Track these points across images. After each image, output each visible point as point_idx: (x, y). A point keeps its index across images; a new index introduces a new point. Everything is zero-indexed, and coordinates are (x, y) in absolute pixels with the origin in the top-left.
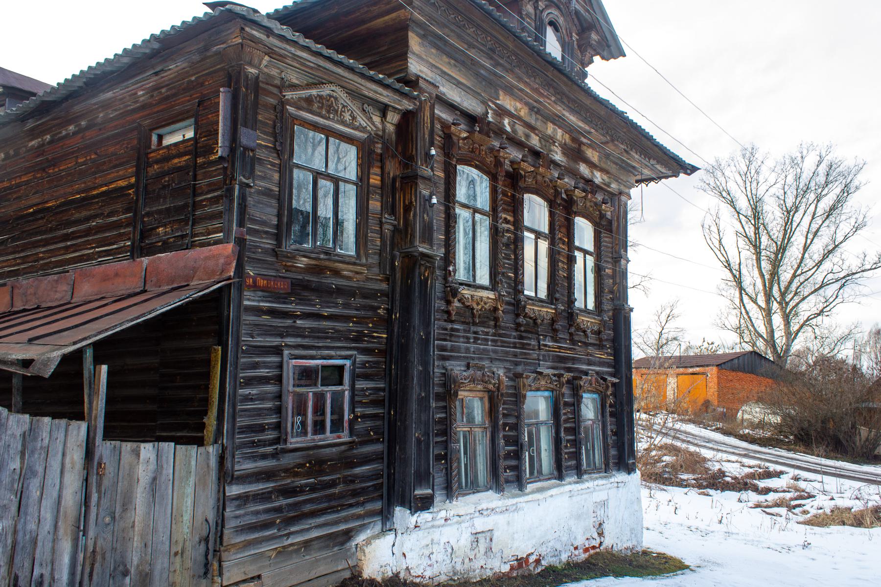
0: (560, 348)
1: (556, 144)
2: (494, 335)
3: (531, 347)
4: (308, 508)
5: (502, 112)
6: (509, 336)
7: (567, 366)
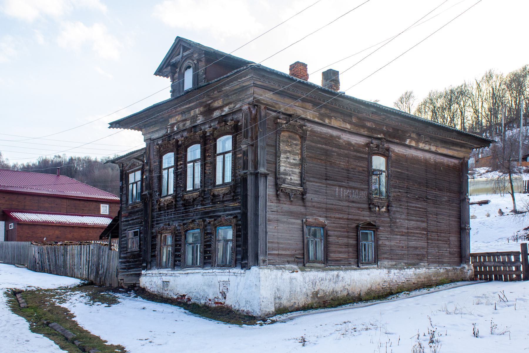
0: (205, 208)
1: (198, 116)
3: (190, 212)
4: (132, 266)
5: (173, 125)
6: (180, 210)
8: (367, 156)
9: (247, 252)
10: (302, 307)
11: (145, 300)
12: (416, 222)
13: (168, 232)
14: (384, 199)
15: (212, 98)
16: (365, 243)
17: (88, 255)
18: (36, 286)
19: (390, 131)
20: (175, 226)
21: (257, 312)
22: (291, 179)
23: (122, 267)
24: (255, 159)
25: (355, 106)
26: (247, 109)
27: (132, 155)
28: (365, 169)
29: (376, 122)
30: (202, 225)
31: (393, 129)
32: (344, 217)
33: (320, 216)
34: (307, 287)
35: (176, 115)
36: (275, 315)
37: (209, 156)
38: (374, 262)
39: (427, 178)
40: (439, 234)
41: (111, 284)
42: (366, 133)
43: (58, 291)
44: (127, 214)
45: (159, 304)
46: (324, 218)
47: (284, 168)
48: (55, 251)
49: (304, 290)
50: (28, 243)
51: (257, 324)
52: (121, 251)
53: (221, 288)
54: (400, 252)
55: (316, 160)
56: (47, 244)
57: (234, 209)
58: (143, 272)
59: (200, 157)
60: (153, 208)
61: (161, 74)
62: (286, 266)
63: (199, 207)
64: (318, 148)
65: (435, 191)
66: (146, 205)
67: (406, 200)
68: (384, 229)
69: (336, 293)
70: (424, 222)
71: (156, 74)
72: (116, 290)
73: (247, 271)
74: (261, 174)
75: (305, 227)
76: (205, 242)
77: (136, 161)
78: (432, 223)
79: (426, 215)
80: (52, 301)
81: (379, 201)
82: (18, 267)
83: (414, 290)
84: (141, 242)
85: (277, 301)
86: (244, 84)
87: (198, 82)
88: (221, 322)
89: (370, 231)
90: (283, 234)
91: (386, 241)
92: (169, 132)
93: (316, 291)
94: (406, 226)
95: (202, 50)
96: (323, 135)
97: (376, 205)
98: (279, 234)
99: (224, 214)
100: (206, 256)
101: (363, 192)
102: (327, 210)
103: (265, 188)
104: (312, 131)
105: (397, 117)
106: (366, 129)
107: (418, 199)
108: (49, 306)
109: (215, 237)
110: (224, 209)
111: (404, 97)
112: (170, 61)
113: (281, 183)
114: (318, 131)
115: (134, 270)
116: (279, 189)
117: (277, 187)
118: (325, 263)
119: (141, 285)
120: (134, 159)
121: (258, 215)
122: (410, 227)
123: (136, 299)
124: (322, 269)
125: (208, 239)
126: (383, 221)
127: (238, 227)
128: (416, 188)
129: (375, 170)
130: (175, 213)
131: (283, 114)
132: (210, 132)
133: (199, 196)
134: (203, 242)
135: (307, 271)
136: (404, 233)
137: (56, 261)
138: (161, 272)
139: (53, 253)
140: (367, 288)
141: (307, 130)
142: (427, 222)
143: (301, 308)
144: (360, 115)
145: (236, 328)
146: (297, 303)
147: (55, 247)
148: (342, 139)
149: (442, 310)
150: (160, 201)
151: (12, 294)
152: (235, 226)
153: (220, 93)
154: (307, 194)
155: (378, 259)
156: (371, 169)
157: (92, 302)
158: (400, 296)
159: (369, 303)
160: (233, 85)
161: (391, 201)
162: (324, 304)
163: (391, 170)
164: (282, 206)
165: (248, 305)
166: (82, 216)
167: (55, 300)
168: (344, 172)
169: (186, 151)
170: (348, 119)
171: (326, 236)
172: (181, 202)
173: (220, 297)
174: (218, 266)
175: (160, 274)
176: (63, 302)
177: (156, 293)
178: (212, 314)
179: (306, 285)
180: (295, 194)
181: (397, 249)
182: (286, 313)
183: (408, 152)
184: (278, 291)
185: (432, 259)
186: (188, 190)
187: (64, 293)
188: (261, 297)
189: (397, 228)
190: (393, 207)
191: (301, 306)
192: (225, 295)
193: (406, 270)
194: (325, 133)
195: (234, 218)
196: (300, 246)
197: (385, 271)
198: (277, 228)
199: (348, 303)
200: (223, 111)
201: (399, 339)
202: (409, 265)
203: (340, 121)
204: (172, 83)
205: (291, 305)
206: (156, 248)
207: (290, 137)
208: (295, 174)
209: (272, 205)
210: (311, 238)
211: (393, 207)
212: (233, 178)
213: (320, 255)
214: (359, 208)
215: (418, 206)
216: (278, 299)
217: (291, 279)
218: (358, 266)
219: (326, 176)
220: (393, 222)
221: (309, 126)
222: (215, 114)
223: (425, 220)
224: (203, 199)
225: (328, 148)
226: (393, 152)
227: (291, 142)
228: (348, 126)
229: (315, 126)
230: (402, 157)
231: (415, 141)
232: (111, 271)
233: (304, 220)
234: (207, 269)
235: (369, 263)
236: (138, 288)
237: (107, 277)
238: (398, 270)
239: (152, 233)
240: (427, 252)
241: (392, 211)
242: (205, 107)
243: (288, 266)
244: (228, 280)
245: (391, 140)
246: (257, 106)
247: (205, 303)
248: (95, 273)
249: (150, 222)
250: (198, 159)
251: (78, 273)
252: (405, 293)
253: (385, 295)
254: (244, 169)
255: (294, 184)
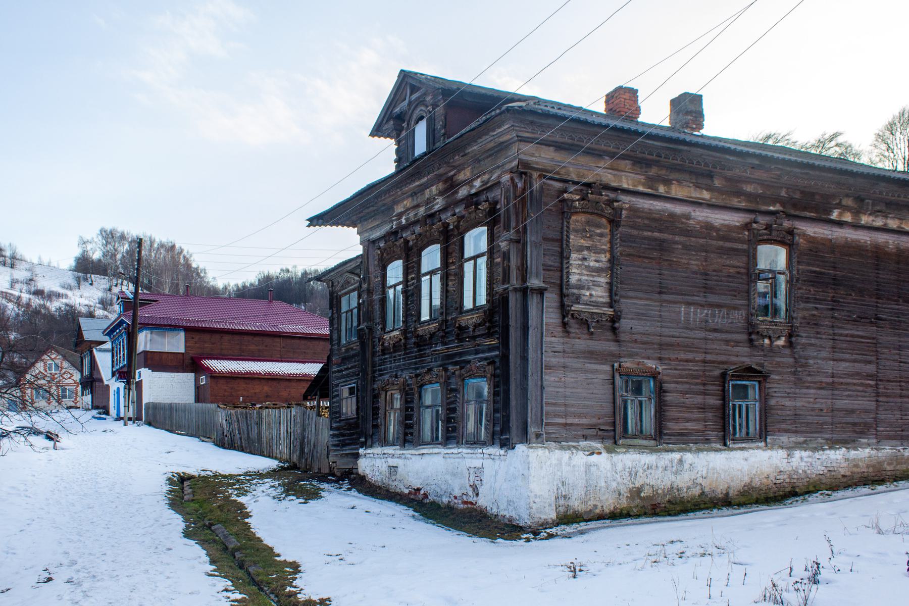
2: (404, 355)
4: (347, 442)
5: (400, 215)
7: (454, 360)
8: (745, 247)
9: (508, 421)
10: (610, 513)
11: (361, 495)
12: (852, 364)
13: (396, 388)
14: (781, 323)
15: (454, 167)
16: (740, 403)
17: (289, 424)
18: (214, 470)
19: (797, 197)
20: (405, 378)
21: (525, 520)
22: (591, 295)
23: (335, 443)
24: (522, 265)
25: (716, 157)
26: (508, 181)
27: (345, 267)
28: (742, 269)
29: (766, 183)
30: (442, 376)
31: (802, 192)
32: (697, 359)
33: (648, 358)
34: (619, 480)
35: (403, 200)
36: (557, 525)
37: (453, 262)
38: (758, 437)
39: (878, 280)
40: (903, 384)
41: (319, 469)
42: (743, 205)
43: (242, 477)
44: (340, 361)
45: (378, 501)
46: (656, 361)
47: (578, 276)
48: (246, 417)
49: (614, 485)
50: (214, 406)
51: (520, 539)
52: (332, 419)
53: (472, 479)
54: (816, 420)
55: (640, 259)
56: (240, 407)
57: (491, 349)
58: (361, 451)
59: (439, 266)
60: (374, 350)
61: (380, 134)
62: (581, 443)
63: (439, 346)
64: (645, 238)
65: (897, 305)
66: (363, 344)
67: (831, 324)
68: (781, 378)
69: (678, 490)
70: (870, 362)
71: (372, 134)
72: (323, 478)
74: (532, 289)
75: (617, 377)
76: (448, 404)
77: (350, 276)
78: (888, 364)
79: (874, 349)
80: (228, 492)
81: (771, 327)
82: (203, 441)
83: (845, 488)
85: (562, 502)
86: (501, 140)
87: (434, 141)
88: (463, 533)
89: (752, 383)
90: (574, 390)
91: (784, 399)
92: (394, 227)
93: (637, 486)
94: (830, 371)
95: (438, 89)
96: (655, 214)
97: (764, 334)
98: (567, 390)
99: (475, 358)
100: (450, 427)
101: (736, 312)
102: (662, 346)
103: (540, 313)
104: (633, 210)
105: (806, 171)
106: (743, 197)
107: (858, 321)
108: (220, 500)
109: (461, 395)
110: (475, 350)
111: (896, 122)
112: (392, 111)
113: (570, 304)
114: (643, 208)
115: (350, 447)
116: (567, 314)
117: (564, 310)
118: (658, 438)
119: (360, 471)
120: (347, 274)
121: (528, 359)
122: (838, 374)
123: (349, 492)
124: (650, 449)
125: (452, 399)
126: (779, 365)
128: (854, 300)
129: (763, 271)
130: (404, 358)
131: (575, 183)
132: (454, 223)
133: (439, 330)
134: (445, 404)
135: (619, 453)
136: (824, 385)
137: (248, 434)
138: (385, 452)
139: (244, 420)
140: (743, 484)
141: (621, 209)
142: (877, 363)
143: (606, 515)
144: (729, 174)
145: (484, 543)
146: (599, 507)
147: (246, 412)
148: (694, 219)
149: (871, 526)
150: (383, 339)
151: (178, 481)
152: (491, 378)
153: (466, 158)
154: (621, 320)
155: (766, 431)
156: (754, 271)
157: (283, 495)
158: (810, 499)
159: (742, 510)
160: (484, 143)
161: (797, 327)
162: (653, 509)
163: (798, 271)
164: (573, 343)
165: (511, 508)
166: (304, 362)
167: (233, 490)
168: (697, 278)
170: (706, 181)
171: (660, 391)
172: (413, 340)
173: (470, 493)
175: (384, 454)
176: (243, 494)
177: (380, 484)
178: (454, 520)
179: (618, 476)
180: (598, 321)
181: (808, 413)
182: (578, 523)
183: (836, 234)
184: (563, 485)
185: (887, 431)
186: (423, 319)
187: (249, 480)
188: (532, 494)
189: (810, 375)
190: (802, 337)
191: (608, 511)
192: (478, 491)
193: (828, 452)
194: (660, 211)
195: (489, 364)
196: (608, 408)
197: (782, 453)
198: (563, 379)
199: (701, 509)
201: (746, 574)
202: (833, 444)
203: (689, 187)
204: (396, 147)
205: (588, 510)
206: (378, 414)
208: (599, 286)
209: (554, 341)
210: (630, 397)
211: (802, 337)
213: (649, 424)
214: (727, 342)
215: (856, 333)
216: (563, 498)
217: (588, 466)
218: (725, 445)
219: (661, 287)
220: (800, 364)
221: (626, 200)
222: (461, 192)
223: (873, 358)
224: (444, 334)
225: (665, 236)
226: (804, 235)
227: (590, 231)
228: (706, 195)
229: (638, 200)
230: (823, 244)
231: (851, 212)
232: (320, 448)
233: (616, 365)
234: (450, 448)
235: (748, 438)
236: (355, 476)
237: (315, 458)
238: (810, 453)
239: (374, 390)
240: (875, 418)
241: (798, 344)
242: (446, 181)
243: (583, 443)
244: (481, 466)
245: (797, 213)
246: (525, 173)
247: (449, 502)
248: (298, 452)
249: (369, 373)
250: (438, 269)
251: (277, 452)
252: (822, 494)
253: (780, 496)
254: (504, 282)
255: (597, 305)
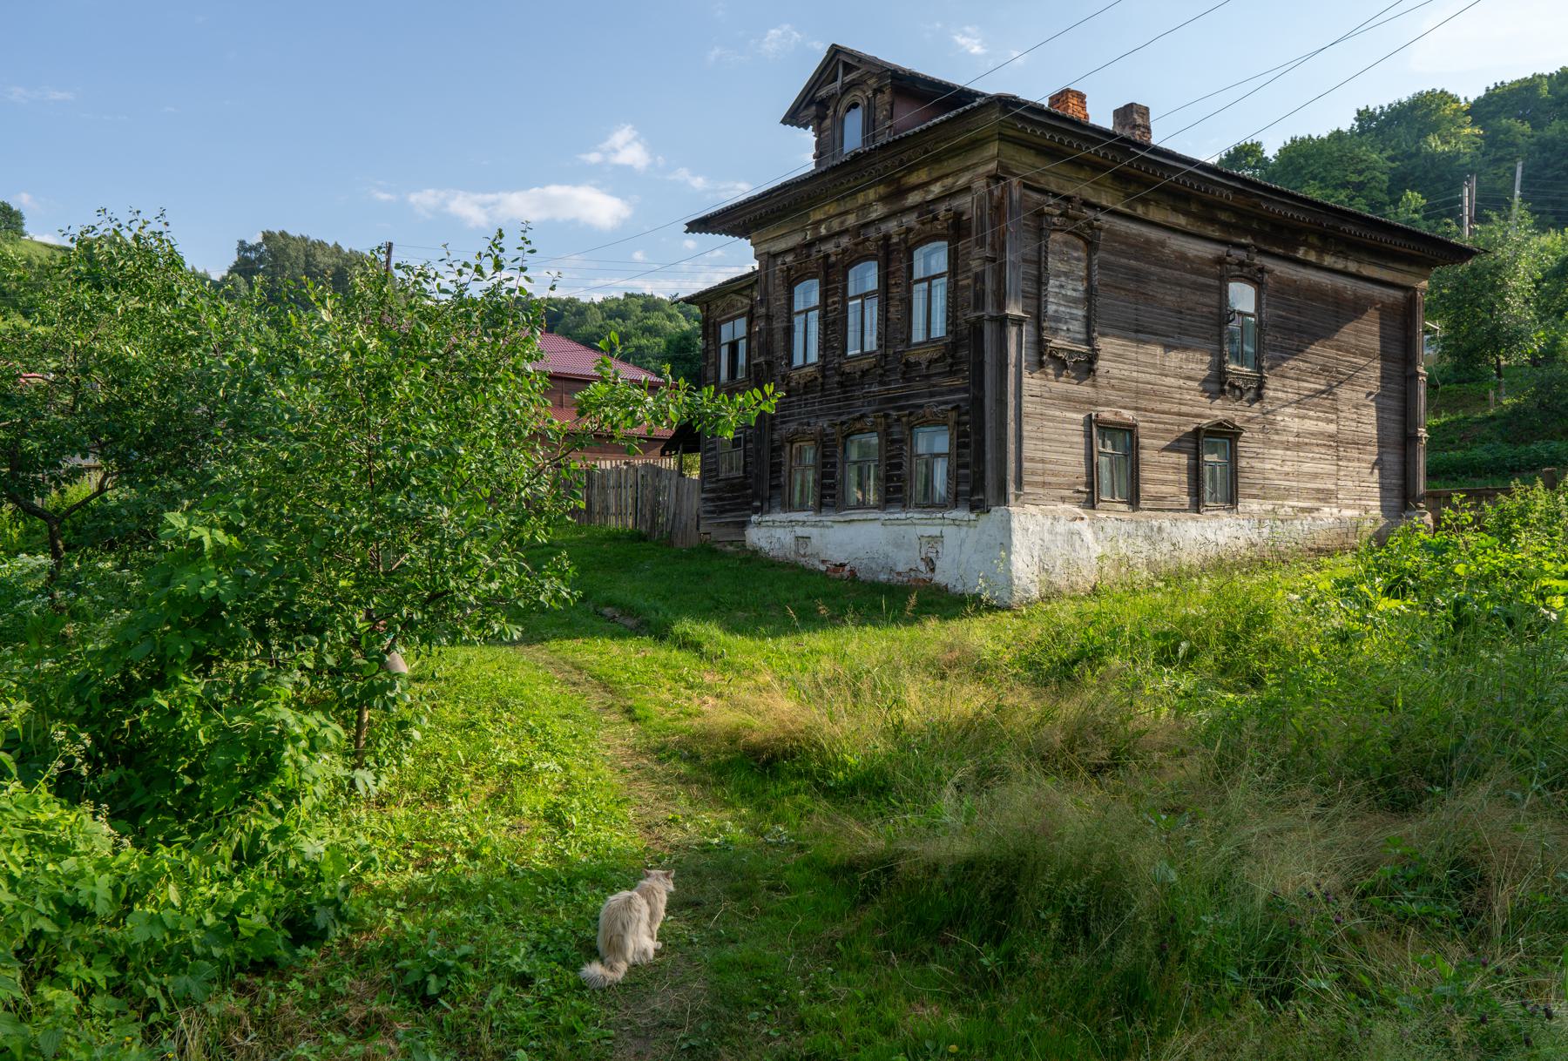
5: (818, 223)
33: (1125, 408)
42: (1217, 234)
58: (754, 518)
59: (876, 287)
64: (1121, 266)
70: (1331, 421)
71: (784, 122)
73: (984, 517)
76: (888, 458)
84: (749, 460)
92: (808, 238)
117: (1040, 344)
127: (962, 428)
131: (1055, 195)
169: (911, 258)
172: (837, 379)
173: (922, 567)
174: (917, 506)
186: (850, 353)
200: (928, 192)
207: (1066, 243)
212: (950, 328)
226: (1270, 272)
239: (772, 441)
246: (1004, 179)
250: (873, 292)
